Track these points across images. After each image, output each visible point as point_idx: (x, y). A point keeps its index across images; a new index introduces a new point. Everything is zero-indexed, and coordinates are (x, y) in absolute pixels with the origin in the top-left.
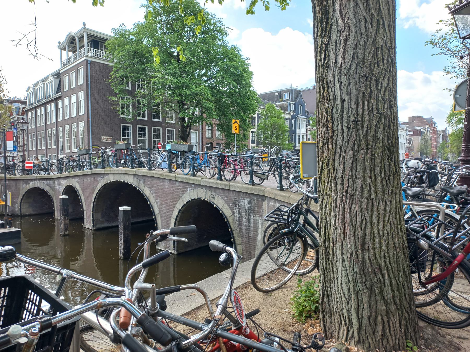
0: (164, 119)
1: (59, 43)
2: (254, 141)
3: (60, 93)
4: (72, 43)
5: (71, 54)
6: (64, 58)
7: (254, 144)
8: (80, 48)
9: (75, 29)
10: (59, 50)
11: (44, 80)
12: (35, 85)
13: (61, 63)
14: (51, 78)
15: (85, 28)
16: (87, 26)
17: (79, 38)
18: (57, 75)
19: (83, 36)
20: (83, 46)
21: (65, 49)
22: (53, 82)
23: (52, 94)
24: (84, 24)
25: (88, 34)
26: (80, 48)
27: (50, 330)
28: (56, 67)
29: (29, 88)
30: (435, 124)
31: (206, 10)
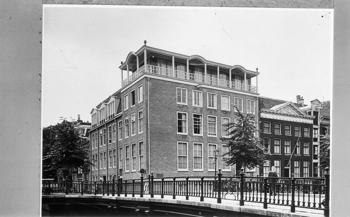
0: (205, 134)
1: (122, 63)
2: (317, 139)
3: (121, 113)
4: (133, 62)
5: (131, 73)
6: (125, 77)
7: (317, 159)
8: (140, 66)
9: (135, 49)
10: (121, 70)
11: (106, 101)
12: (98, 107)
13: (122, 83)
14: (113, 99)
15: (145, 46)
16: (147, 45)
17: (139, 57)
18: (118, 95)
19: (143, 54)
20: (143, 64)
21: (126, 69)
22: (114, 103)
23: (114, 114)
24: (145, 42)
25: (147, 52)
26: (140, 66)
27: (259, 184)
28: (117, 87)
29: (93, 110)
30: (51, 126)
31: (307, 102)
